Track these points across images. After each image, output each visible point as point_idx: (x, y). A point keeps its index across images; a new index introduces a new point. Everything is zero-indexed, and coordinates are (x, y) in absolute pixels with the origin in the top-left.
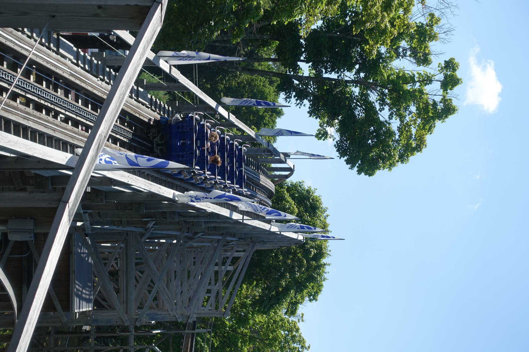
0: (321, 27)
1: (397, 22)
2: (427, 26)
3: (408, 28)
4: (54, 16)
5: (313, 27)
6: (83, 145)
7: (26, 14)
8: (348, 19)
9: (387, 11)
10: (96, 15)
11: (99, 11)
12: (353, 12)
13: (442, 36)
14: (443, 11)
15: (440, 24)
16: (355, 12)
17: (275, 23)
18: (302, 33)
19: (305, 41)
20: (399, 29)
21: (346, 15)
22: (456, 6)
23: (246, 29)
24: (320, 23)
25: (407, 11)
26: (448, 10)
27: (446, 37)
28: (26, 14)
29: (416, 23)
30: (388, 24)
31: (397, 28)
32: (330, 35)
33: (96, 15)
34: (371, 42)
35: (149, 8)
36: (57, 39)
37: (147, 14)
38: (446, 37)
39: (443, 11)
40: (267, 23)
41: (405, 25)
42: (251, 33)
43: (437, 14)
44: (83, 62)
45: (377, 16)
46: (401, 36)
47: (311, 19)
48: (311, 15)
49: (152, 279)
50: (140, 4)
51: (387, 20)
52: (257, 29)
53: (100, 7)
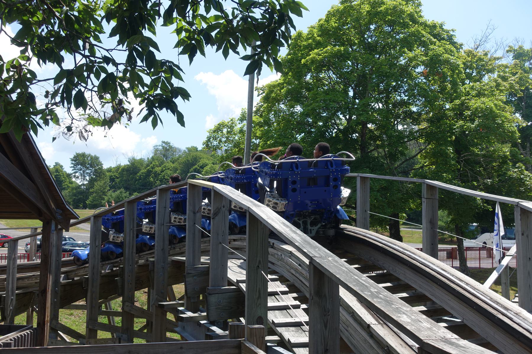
0: (520, 114)
1: (514, 71)
2: (514, 53)
3: (517, 65)
4: (530, 259)
5: (520, 119)
6: (271, 303)
7: (529, 273)
8: (513, 99)
9: (508, 79)
10: (527, 236)
11: (525, 235)
12: (509, 97)
13: (520, 44)
14: (505, 46)
15: (511, 44)
16: (509, 95)
17: (520, 141)
18: (524, 125)
19: (529, 122)
20: (517, 69)
21: (511, 100)
22: (502, 39)
23: (524, 156)
24: (517, 115)
25: (507, 67)
26: (504, 43)
27: (521, 41)
28: (529, 273)
29: (513, 60)
30: (516, 76)
31: (517, 71)
32: (524, 108)
33: (527, 236)
34: (527, 85)
35: (521, 209)
36: (309, 265)
37: (525, 210)
38: (521, 41)
39: (505, 46)
40: (519, 145)
41: (515, 67)
42: (526, 153)
43: (508, 49)
44: (283, 243)
45: (510, 83)
46: (522, 68)
47: (516, 120)
48: (514, 121)
49: (293, 298)
50: (519, 213)
51: (513, 78)
52: (524, 151)
53: (523, 234)
